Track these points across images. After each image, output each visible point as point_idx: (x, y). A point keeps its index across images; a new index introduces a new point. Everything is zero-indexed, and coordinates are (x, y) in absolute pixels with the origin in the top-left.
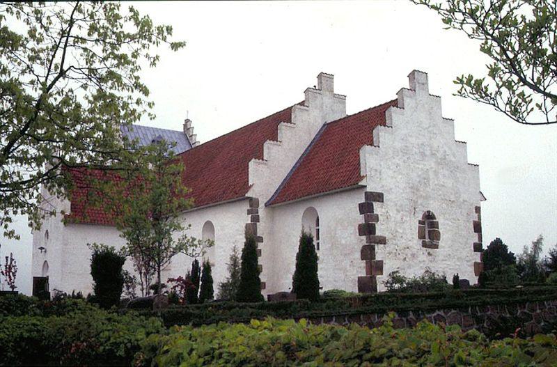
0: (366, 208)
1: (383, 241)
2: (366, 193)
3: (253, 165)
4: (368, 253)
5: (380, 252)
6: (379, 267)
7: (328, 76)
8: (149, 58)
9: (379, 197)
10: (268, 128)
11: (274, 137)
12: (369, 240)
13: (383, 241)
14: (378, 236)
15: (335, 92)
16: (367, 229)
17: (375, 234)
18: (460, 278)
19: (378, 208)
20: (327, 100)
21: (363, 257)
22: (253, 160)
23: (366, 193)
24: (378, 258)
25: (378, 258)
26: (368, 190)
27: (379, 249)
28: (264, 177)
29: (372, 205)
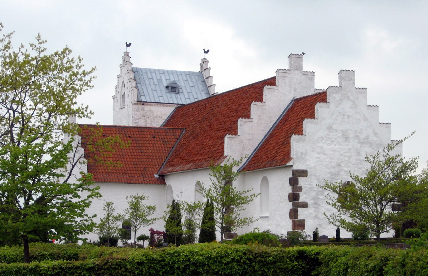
0: (293, 182)
1: (305, 205)
2: (293, 171)
3: (227, 139)
4: (294, 214)
5: (302, 213)
6: (301, 225)
7: (284, 71)
8: (93, 217)
9: (304, 173)
10: (254, 92)
11: (260, 98)
12: (294, 205)
13: (305, 205)
14: (300, 202)
15: (304, 70)
16: (294, 197)
17: (298, 200)
18: (320, 235)
19: (302, 181)
20: (296, 76)
21: (291, 217)
22: (227, 136)
23: (293, 171)
24: (300, 217)
25: (300, 217)
26: (295, 168)
27: (301, 210)
28: (238, 147)
29: (298, 179)
